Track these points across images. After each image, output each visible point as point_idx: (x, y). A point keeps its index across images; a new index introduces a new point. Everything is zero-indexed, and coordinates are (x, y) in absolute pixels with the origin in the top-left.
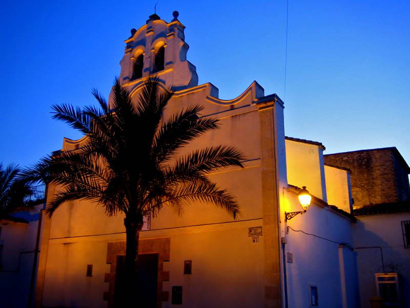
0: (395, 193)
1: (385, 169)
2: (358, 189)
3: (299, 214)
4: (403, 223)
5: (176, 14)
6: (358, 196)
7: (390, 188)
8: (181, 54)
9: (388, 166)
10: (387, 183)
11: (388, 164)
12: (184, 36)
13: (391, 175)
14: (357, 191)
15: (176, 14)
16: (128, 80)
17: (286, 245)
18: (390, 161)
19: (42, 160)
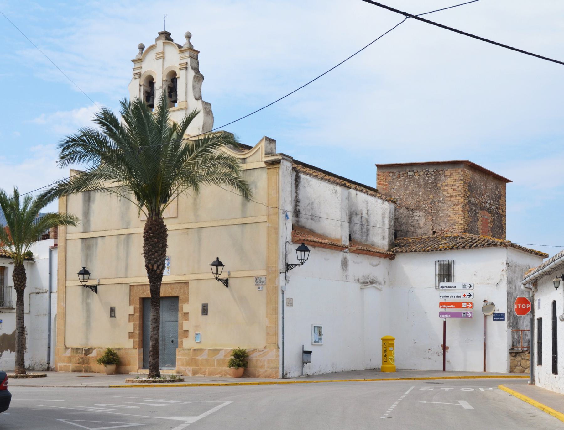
0: (462, 220)
1: (454, 190)
2: (421, 214)
3: (298, 266)
4: (437, 263)
5: (189, 37)
6: (420, 222)
7: (457, 213)
8: (194, 88)
9: (458, 187)
10: (454, 207)
11: (458, 184)
12: (198, 63)
13: (460, 198)
14: (419, 216)
15: (189, 37)
16: (149, 90)
17: (285, 293)
18: (461, 180)
19: (57, 162)
